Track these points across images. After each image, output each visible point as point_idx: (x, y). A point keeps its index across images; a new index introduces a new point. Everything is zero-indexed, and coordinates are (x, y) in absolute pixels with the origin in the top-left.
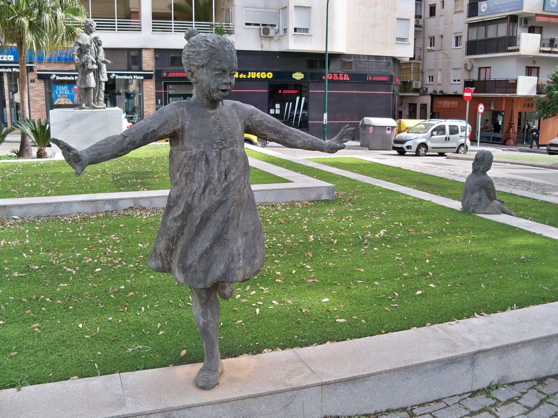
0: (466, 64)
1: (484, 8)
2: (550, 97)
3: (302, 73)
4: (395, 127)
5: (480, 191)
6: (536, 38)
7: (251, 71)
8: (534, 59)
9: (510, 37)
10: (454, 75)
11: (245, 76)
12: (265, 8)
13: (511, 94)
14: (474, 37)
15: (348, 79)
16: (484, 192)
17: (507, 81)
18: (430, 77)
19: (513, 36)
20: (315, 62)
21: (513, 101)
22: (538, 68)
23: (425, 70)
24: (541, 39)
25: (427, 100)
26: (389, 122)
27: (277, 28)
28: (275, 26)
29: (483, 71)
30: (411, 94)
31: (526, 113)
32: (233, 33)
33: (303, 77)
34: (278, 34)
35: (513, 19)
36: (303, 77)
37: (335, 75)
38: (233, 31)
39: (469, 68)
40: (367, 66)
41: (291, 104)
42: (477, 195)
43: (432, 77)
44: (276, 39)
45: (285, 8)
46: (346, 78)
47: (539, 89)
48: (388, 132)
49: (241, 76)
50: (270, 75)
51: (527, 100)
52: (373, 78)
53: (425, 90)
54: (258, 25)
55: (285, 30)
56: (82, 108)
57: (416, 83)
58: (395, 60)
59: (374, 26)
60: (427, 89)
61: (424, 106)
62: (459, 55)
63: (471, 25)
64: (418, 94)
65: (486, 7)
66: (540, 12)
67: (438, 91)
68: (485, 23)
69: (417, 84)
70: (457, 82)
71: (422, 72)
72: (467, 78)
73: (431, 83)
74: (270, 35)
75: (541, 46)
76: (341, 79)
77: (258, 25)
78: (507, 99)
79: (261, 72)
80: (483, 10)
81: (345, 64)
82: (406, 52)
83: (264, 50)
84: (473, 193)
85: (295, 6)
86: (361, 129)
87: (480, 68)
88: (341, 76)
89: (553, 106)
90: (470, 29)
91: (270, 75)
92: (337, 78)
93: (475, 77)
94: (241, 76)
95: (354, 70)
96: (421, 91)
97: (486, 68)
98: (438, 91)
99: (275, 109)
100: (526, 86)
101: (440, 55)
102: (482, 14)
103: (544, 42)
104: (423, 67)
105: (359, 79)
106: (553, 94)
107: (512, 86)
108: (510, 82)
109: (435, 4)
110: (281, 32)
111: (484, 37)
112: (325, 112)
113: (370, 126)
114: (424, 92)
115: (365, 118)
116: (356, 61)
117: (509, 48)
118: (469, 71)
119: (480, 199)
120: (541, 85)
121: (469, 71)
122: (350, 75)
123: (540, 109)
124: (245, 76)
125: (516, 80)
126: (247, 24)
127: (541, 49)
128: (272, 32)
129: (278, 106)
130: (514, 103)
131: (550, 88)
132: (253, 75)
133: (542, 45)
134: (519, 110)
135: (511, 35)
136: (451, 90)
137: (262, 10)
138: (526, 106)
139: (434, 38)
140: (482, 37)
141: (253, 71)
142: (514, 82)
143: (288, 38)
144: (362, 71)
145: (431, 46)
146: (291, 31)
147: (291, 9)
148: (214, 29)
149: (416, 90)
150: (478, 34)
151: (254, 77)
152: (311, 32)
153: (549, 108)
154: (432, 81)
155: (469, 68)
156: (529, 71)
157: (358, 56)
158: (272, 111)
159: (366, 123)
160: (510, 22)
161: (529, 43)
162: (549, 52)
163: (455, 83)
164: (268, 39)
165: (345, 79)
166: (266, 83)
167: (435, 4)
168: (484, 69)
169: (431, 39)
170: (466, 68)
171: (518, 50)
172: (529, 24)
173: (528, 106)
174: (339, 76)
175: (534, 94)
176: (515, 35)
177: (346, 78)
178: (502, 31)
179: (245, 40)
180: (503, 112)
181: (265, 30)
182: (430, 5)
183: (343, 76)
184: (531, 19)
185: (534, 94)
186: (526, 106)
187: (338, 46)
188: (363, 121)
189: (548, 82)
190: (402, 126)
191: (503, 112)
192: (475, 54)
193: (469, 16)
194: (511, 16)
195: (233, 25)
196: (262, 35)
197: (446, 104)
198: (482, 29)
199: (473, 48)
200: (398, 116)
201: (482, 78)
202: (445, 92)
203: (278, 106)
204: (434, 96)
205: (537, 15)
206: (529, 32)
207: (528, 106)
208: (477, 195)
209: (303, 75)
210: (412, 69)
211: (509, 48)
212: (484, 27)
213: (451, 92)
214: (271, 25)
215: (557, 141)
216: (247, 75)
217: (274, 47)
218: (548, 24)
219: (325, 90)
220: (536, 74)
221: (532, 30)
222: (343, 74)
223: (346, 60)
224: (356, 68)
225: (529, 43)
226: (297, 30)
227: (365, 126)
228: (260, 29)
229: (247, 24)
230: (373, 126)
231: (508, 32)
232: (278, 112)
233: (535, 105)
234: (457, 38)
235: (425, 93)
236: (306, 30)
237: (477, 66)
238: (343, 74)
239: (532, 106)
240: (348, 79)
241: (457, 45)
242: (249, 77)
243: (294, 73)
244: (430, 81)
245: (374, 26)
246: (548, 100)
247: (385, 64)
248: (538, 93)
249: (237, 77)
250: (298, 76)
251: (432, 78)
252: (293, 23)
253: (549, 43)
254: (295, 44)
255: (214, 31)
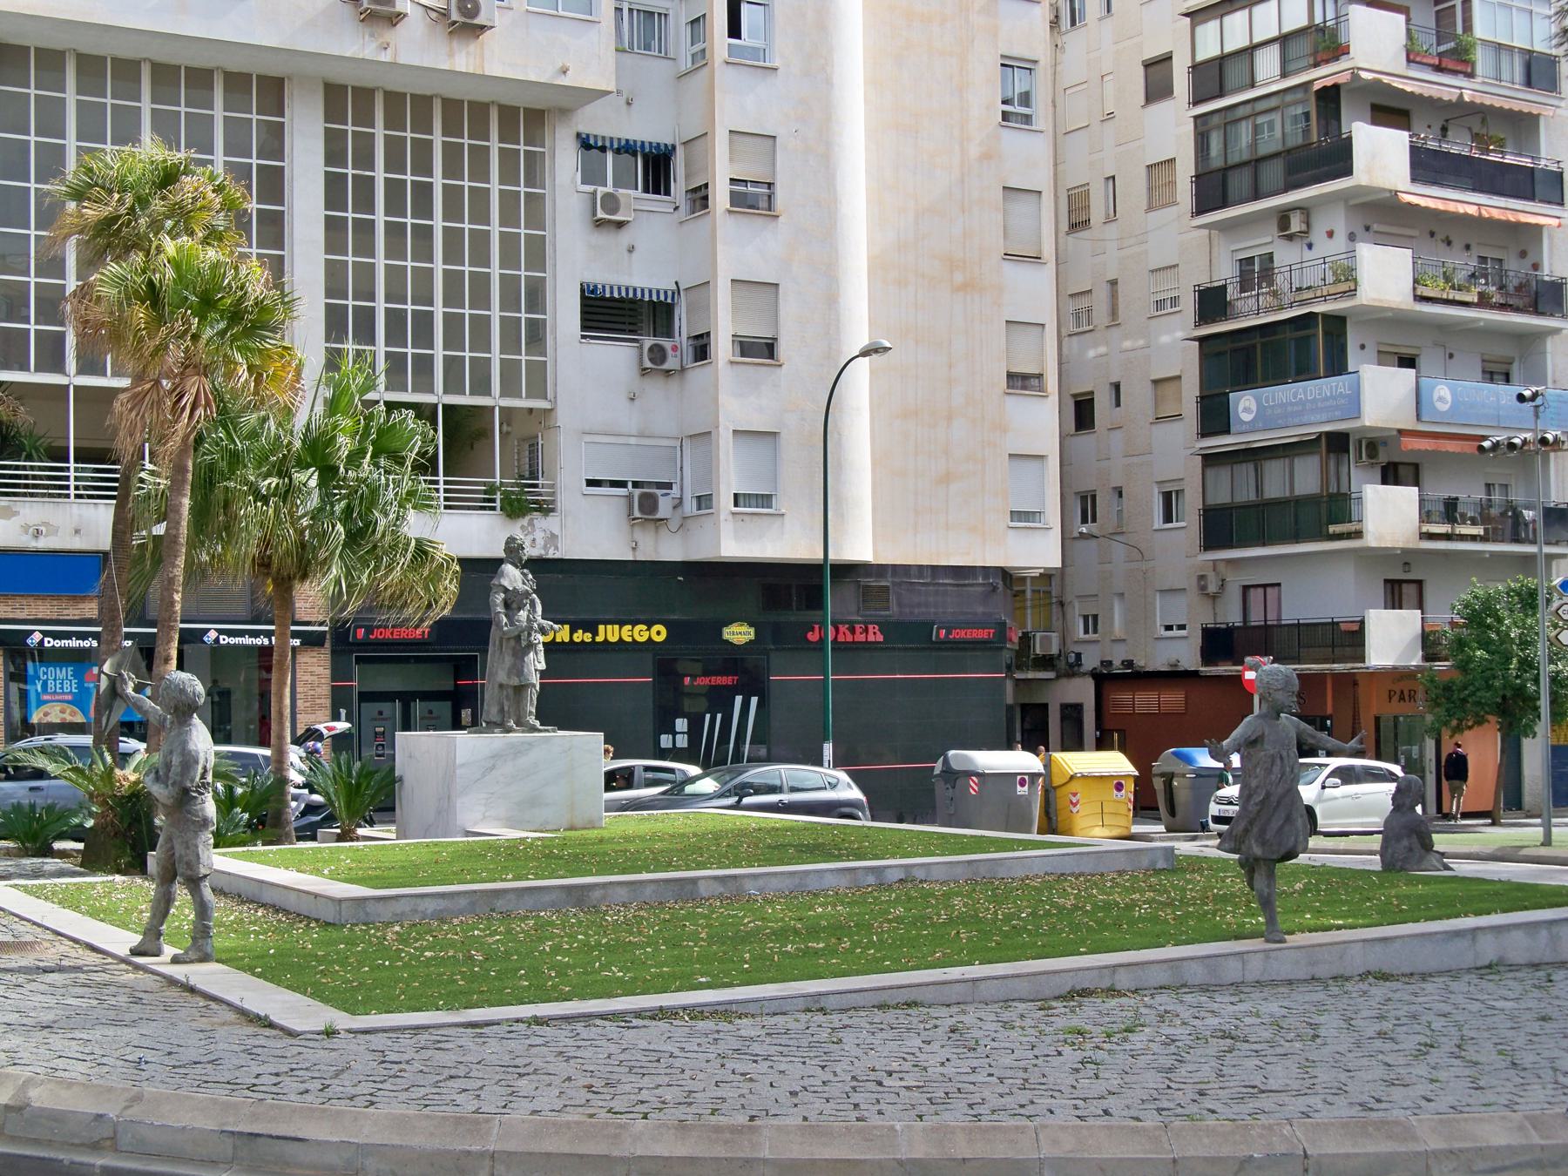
0: (1202, 577)
1: (1246, 410)
2: (1463, 667)
3: (751, 625)
4: (1039, 775)
5: (1409, 836)
6: (1406, 497)
7: (606, 623)
8: (1406, 557)
9: (1331, 496)
10: (1163, 610)
11: (588, 637)
12: (641, 435)
13: (1349, 665)
14: (1221, 496)
15: (880, 638)
16: (1414, 839)
17: (1334, 624)
18: (1086, 618)
19: (1339, 494)
20: (790, 589)
21: (1355, 684)
22: (1419, 583)
23: (1068, 598)
24: (1422, 501)
25: (1082, 691)
26: (1020, 761)
27: (675, 491)
28: (669, 486)
29: (1256, 596)
30: (1030, 675)
31: (1396, 718)
32: (553, 510)
33: (752, 637)
34: (679, 510)
35: (1337, 443)
36: (752, 637)
37: (843, 628)
38: (553, 502)
39: (1212, 588)
40: (931, 599)
41: (719, 716)
42: (1405, 843)
43: (1095, 617)
44: (674, 525)
45: (705, 437)
46: (875, 636)
47: (1429, 643)
48: (1022, 790)
49: (579, 636)
50: (658, 633)
51: (1397, 677)
52: (948, 633)
53: (1072, 658)
54: (622, 484)
55: (704, 501)
56: (509, 730)
57: (1042, 638)
58: (1006, 575)
59: (946, 479)
60: (1078, 656)
61: (1072, 713)
62: (1179, 547)
63: (1210, 460)
64: (1051, 675)
65: (1254, 408)
66: (1409, 423)
67: (1117, 663)
68: (1254, 455)
69: (1046, 641)
70: (1175, 633)
71: (1062, 604)
72: (1209, 621)
73: (1091, 636)
74: (658, 516)
75: (1422, 521)
76: (861, 638)
77: (622, 484)
78: (1338, 678)
79: (634, 623)
80: (1246, 417)
81: (870, 596)
82: (1038, 551)
83: (640, 557)
84: (1398, 840)
85: (735, 432)
86: (940, 787)
87: (1246, 588)
88: (858, 630)
89: (1473, 693)
90: (1210, 472)
91: (659, 633)
92: (850, 638)
93: (1233, 617)
94: (579, 636)
95: (893, 611)
96: (1062, 665)
97: (1265, 586)
98: (1117, 663)
99: (674, 733)
100: (1391, 638)
101: (1118, 551)
102: (1244, 428)
103: (1428, 507)
104: (1063, 586)
105: (912, 637)
106: (1470, 659)
107: (1352, 639)
108: (1343, 627)
109: (1092, 393)
110: (690, 507)
111: (1253, 497)
112: (826, 739)
113: (969, 774)
114: (1071, 666)
115: (951, 753)
116: (900, 584)
117: (1332, 529)
118: (1214, 598)
119: (1411, 850)
120: (1434, 632)
121: (1214, 598)
122: (884, 627)
123: (1438, 705)
124: (588, 637)
125: (1362, 623)
126: (591, 483)
127: (1424, 529)
128: (664, 508)
129: (681, 724)
130: (1361, 690)
131: (1460, 644)
132: (610, 633)
133: (1426, 516)
134: (1375, 711)
135: (1333, 489)
136: (1157, 659)
137: (633, 441)
138: (1396, 698)
139: (1094, 498)
140: (1247, 494)
141: (612, 623)
142: (1355, 627)
143: (717, 525)
144: (919, 614)
145: (1084, 521)
146: (725, 502)
147: (725, 440)
148: (498, 496)
149: (1046, 662)
150: (1233, 488)
151: (613, 639)
152: (780, 505)
153: (1464, 701)
154: (1095, 631)
155: (1212, 588)
156: (1396, 594)
157: (906, 569)
158: (665, 741)
159: (955, 766)
160: (1329, 451)
161: (1389, 514)
162: (1447, 537)
163: (1170, 633)
164: (651, 526)
165: (871, 638)
166: (648, 658)
167: (1092, 393)
168: (1261, 590)
169: (1084, 499)
170: (1203, 588)
171: (1358, 534)
172: (1383, 458)
173: (1402, 698)
174: (853, 631)
175: (1416, 660)
176: (1344, 490)
177: (875, 636)
178: (1307, 478)
179: (589, 530)
180: (1330, 717)
181: (646, 503)
182: (1074, 396)
183: (866, 630)
184: (1385, 443)
185: (1416, 660)
186: (1396, 698)
187: (859, 544)
188: (946, 761)
189: (1453, 624)
190: (1054, 769)
191: (1330, 717)
192: (1231, 546)
193: (1204, 434)
194: (1329, 434)
195: (552, 486)
196: (637, 514)
197: (1145, 701)
198: (1246, 471)
199: (1221, 527)
200: (1034, 739)
201: (1256, 618)
202: (1142, 663)
203: (681, 724)
204: (1104, 679)
205: (1400, 432)
206: (1384, 482)
207: (1402, 698)
208: (1405, 843)
209: (752, 630)
210: (1029, 594)
211: (1332, 529)
212: (1251, 467)
213: (1159, 663)
214: (660, 485)
215: (1435, 1173)
216: (595, 633)
217: (670, 549)
218: (1435, 455)
219: (825, 674)
220: (1415, 601)
221: (1391, 474)
222: (866, 624)
223: (872, 582)
224: (900, 605)
225: (1389, 514)
226: (741, 500)
227: (953, 776)
228: (630, 497)
229: (591, 483)
230: (978, 775)
231: (1325, 480)
232: (682, 741)
233: (1420, 695)
234: (1167, 497)
235: (1072, 669)
236: (765, 500)
237: (1236, 581)
238: (866, 624)
239: (1412, 697)
240: (880, 638)
241: (1168, 518)
242: (600, 639)
243: (727, 624)
244: (1086, 632)
245: (946, 479)
246: (1458, 678)
247: (980, 589)
248: (1426, 658)
249: (567, 640)
250: (739, 633)
251: (1092, 622)
252: (731, 477)
253: (1442, 508)
254: (735, 542)
255: (498, 504)
